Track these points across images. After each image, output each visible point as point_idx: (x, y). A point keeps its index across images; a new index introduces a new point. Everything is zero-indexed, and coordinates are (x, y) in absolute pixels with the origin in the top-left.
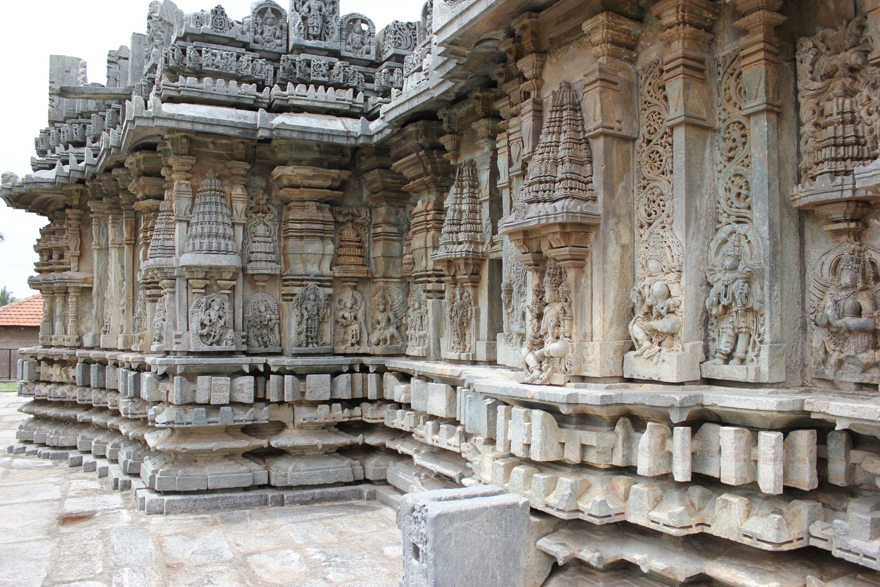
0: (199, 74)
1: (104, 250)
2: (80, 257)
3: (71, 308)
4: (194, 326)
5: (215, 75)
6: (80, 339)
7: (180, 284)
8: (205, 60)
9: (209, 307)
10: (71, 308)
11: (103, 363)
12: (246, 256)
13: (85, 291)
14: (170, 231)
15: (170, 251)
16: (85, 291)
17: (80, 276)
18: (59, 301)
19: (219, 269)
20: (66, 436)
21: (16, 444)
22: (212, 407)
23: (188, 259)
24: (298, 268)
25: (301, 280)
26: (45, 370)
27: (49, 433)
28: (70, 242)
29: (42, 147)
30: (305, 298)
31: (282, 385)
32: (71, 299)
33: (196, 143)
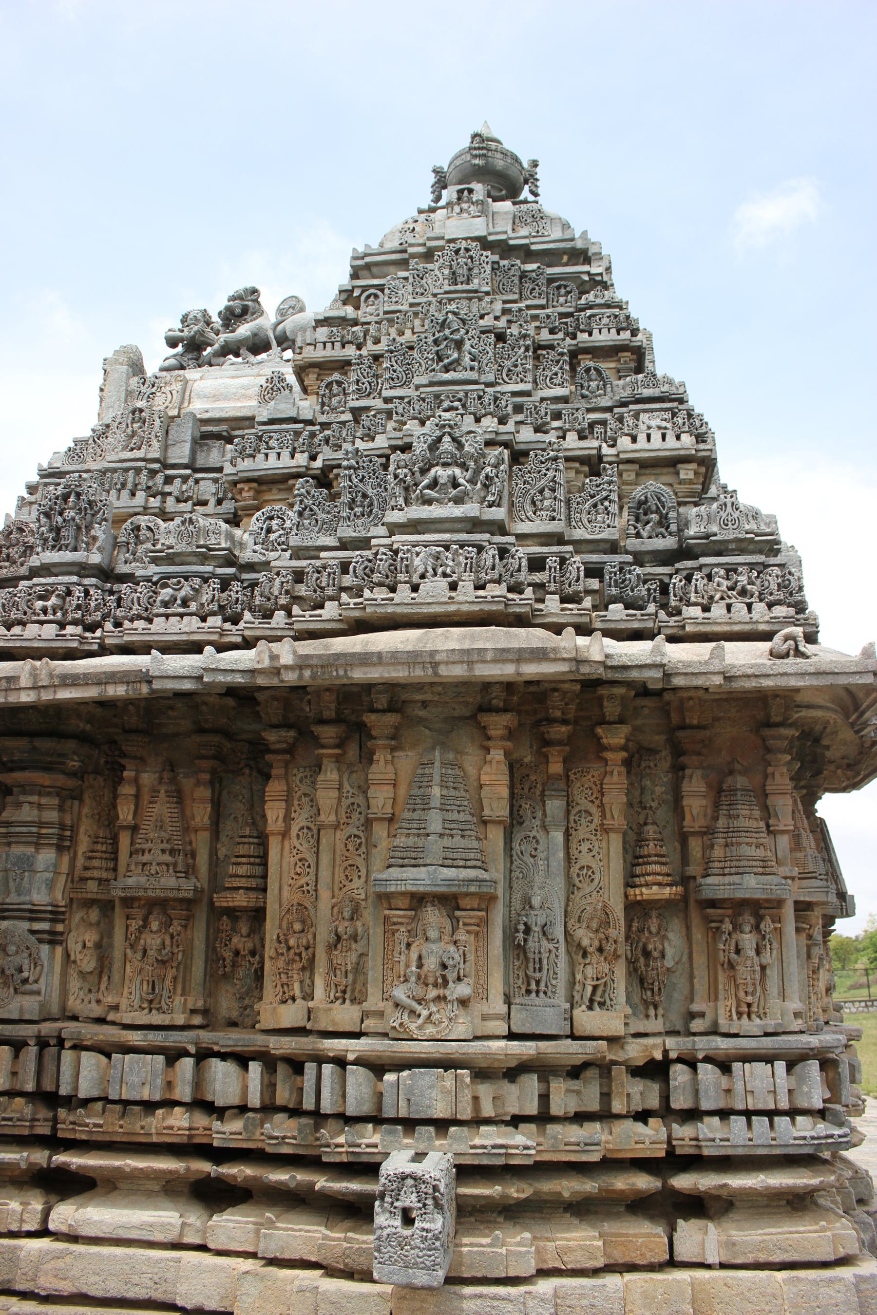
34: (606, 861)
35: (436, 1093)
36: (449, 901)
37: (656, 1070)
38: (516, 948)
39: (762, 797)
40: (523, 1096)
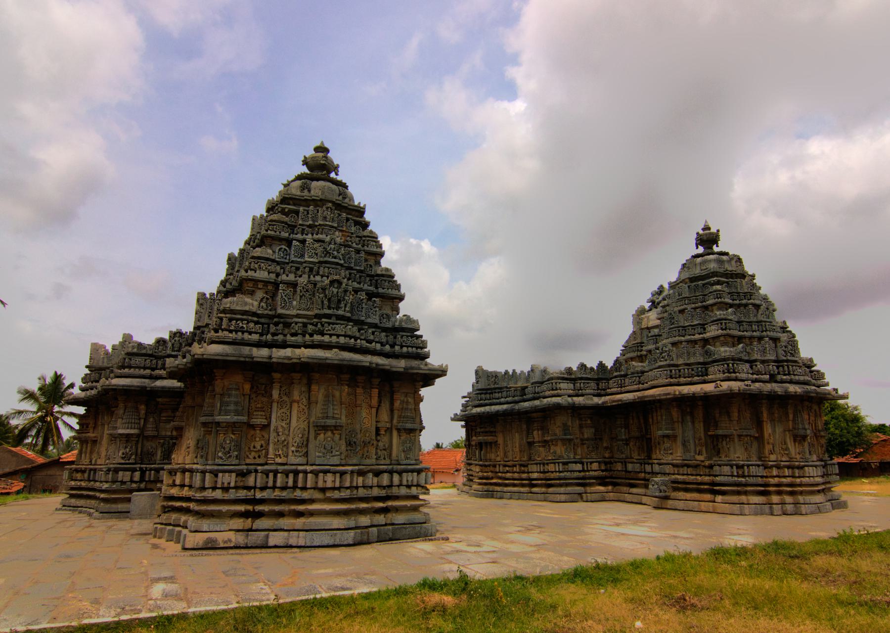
0: (130, 367)
1: (103, 425)
2: (94, 428)
3: (89, 449)
4: (121, 452)
5: (135, 368)
6: (91, 461)
7: (118, 440)
8: (133, 362)
9: (126, 447)
10: (89, 449)
11: (95, 470)
12: (142, 430)
13: (95, 442)
14: (116, 421)
15: (116, 428)
16: (95, 442)
17: (94, 435)
18: (84, 446)
19: (132, 434)
20: (81, 502)
21: (60, 507)
22: (123, 483)
23: (120, 431)
24: (163, 433)
25: (164, 437)
26: (75, 475)
27: (73, 501)
28: (91, 422)
29: (201, 301)
30: (164, 444)
31: (150, 475)
32: (89, 445)
33: (127, 392)
34: (700, 427)
35: (668, 469)
36: (668, 436)
37: (711, 467)
38: (684, 444)
39: (729, 416)
40: (685, 470)
